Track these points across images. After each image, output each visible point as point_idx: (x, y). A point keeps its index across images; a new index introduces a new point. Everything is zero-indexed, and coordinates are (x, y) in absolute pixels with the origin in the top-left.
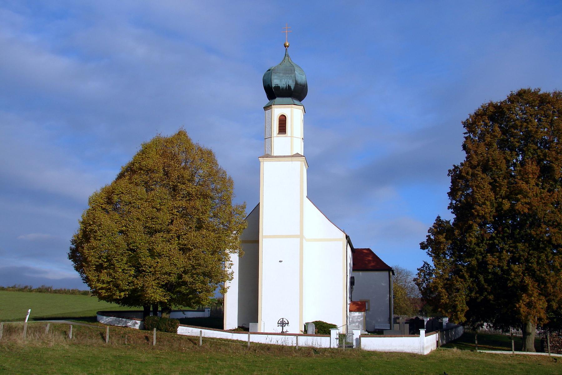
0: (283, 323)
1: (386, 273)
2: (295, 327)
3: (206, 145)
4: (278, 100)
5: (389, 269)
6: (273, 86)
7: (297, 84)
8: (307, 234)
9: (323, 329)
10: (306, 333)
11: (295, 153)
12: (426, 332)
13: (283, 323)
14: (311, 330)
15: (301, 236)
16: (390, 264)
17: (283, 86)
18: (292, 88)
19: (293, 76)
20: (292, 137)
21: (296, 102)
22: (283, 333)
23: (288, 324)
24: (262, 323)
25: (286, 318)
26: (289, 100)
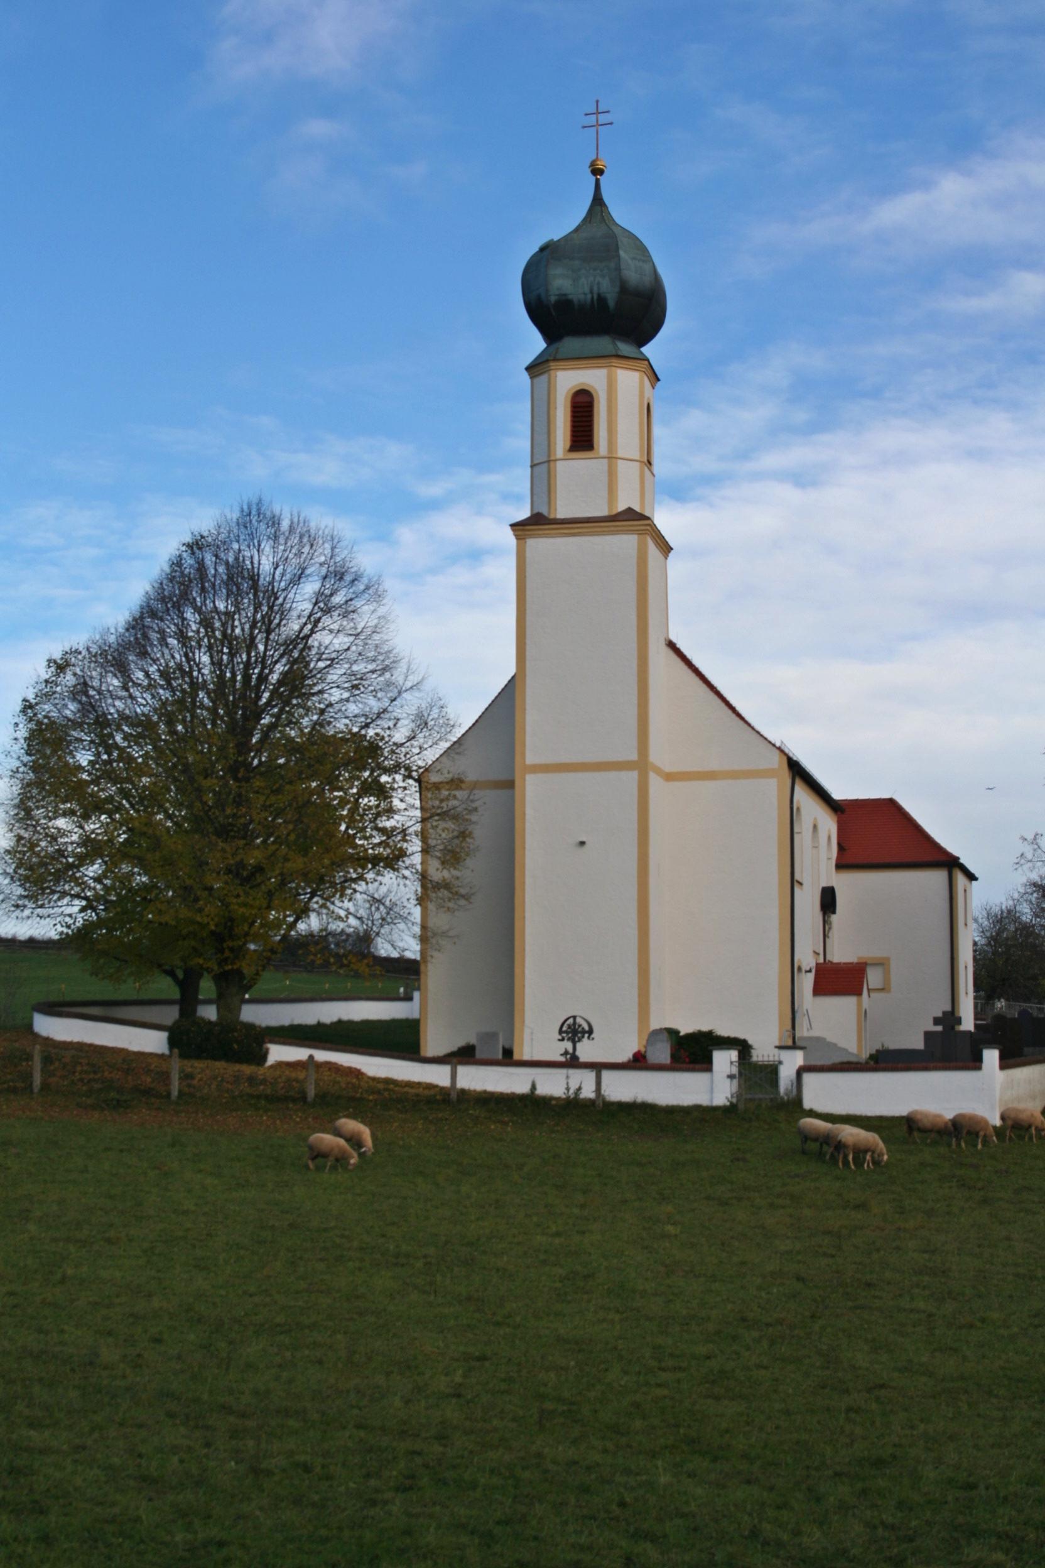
0: (574, 1031)
1: (936, 878)
2: (616, 1040)
3: (335, 1019)
4: (570, 344)
5: (950, 864)
6: (553, 299)
7: (624, 289)
8: (660, 755)
9: (693, 1051)
10: (639, 1062)
11: (621, 507)
12: (1002, 1058)
13: (574, 1031)
14: (662, 1053)
15: (641, 765)
16: (951, 846)
17: (582, 297)
18: (611, 303)
19: (612, 265)
20: (612, 458)
21: (625, 348)
22: (572, 1062)
23: (590, 1032)
24: (527, 1032)
25: (585, 1012)
26: (603, 343)
